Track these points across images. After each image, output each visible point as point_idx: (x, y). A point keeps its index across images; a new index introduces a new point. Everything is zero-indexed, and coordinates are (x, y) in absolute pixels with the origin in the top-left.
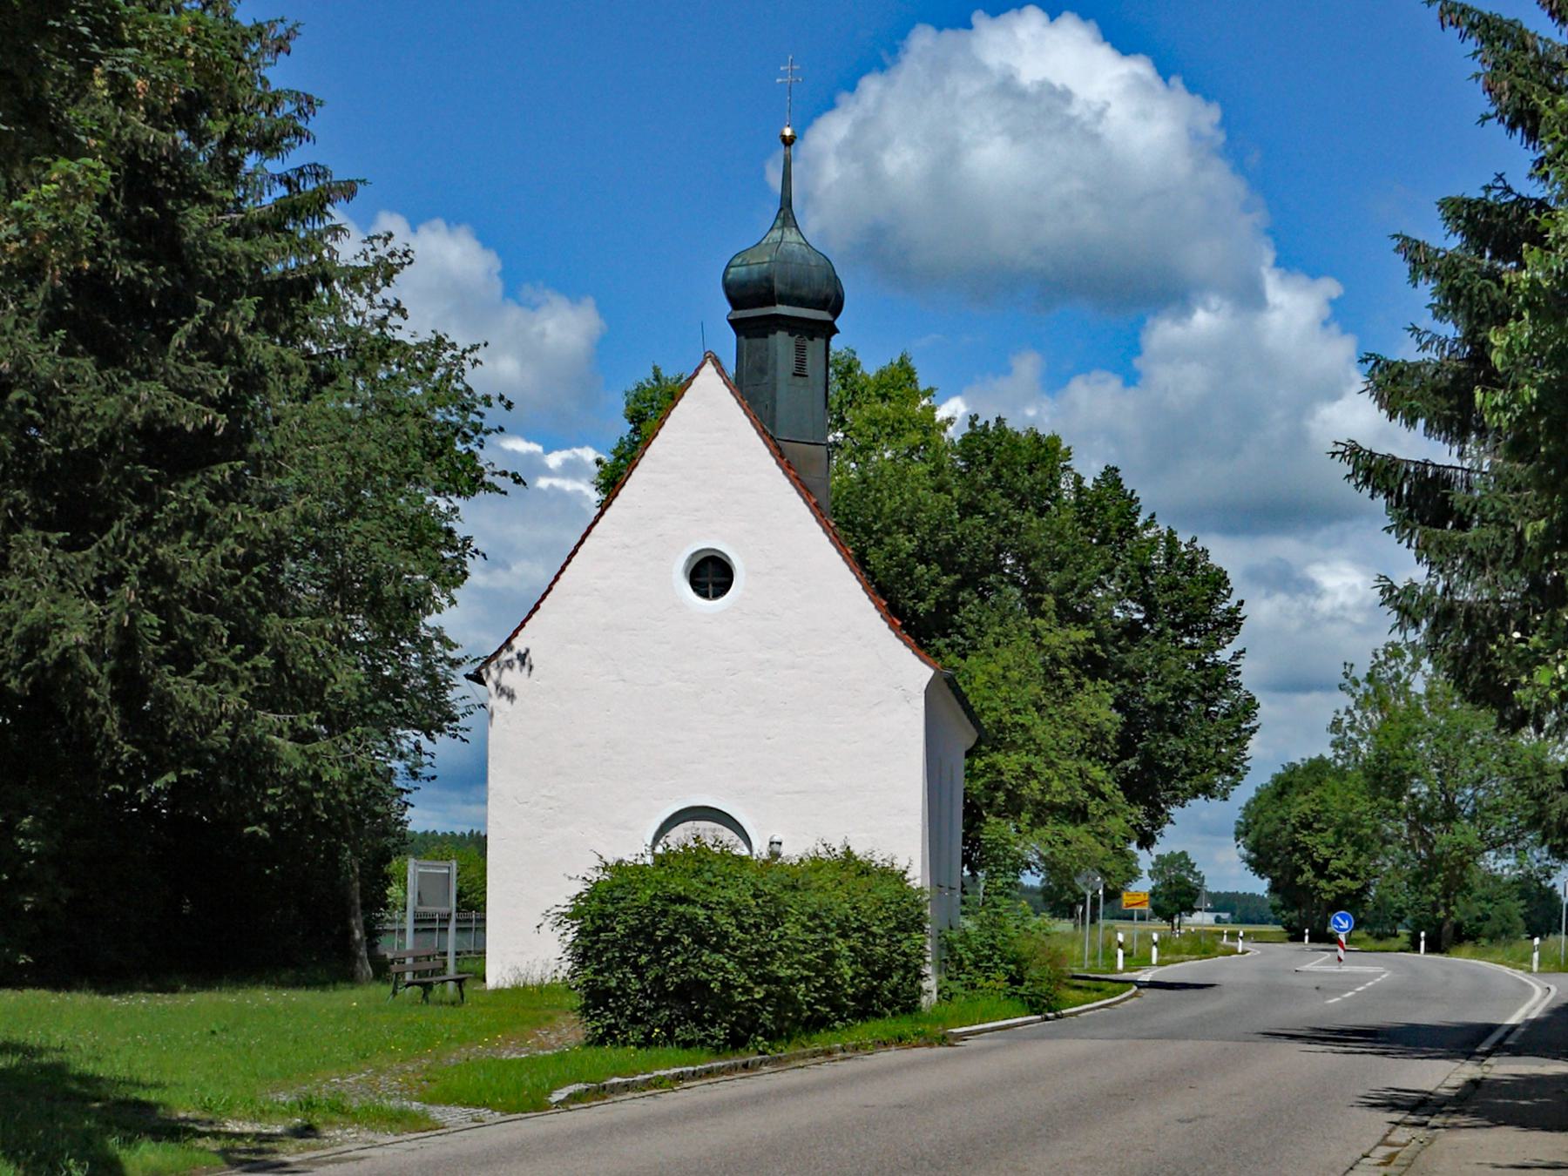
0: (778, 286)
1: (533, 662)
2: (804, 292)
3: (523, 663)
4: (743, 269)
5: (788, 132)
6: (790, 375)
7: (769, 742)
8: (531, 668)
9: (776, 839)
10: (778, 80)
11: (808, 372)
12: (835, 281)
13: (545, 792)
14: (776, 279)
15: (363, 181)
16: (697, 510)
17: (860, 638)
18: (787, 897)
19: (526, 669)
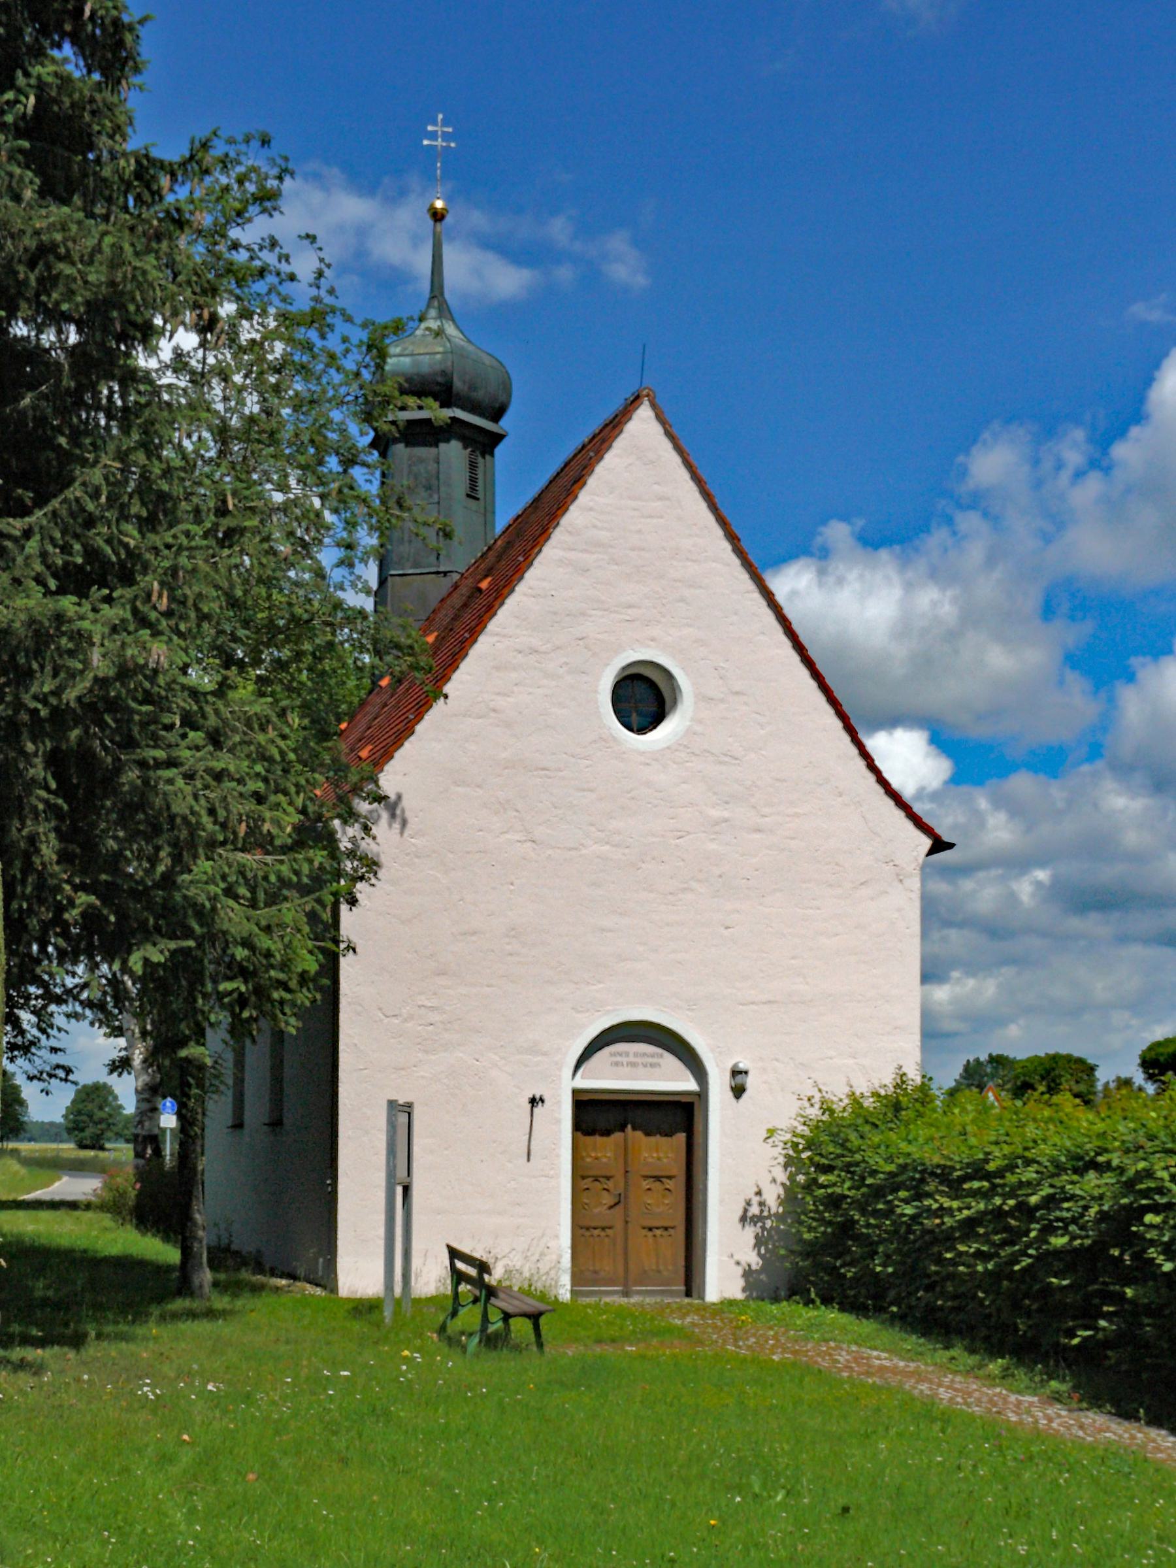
0: (458, 384)
1: (408, 814)
2: (480, 395)
3: (393, 816)
4: (407, 360)
5: (439, 204)
6: (464, 496)
7: (726, 933)
8: (404, 823)
9: (742, 1066)
10: (426, 142)
11: (480, 495)
12: (507, 387)
13: (422, 999)
14: (455, 376)
15: (153, 145)
16: (630, 607)
17: (840, 795)
18: (993, 1148)
19: (397, 826)
